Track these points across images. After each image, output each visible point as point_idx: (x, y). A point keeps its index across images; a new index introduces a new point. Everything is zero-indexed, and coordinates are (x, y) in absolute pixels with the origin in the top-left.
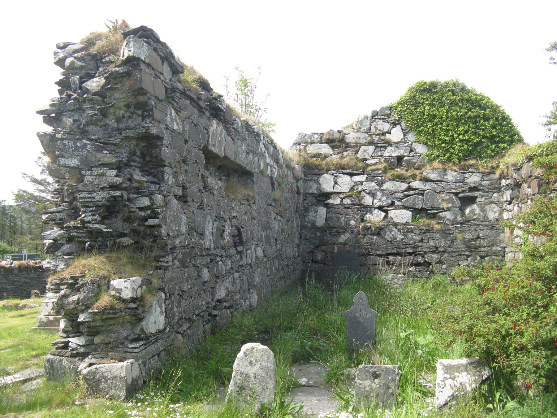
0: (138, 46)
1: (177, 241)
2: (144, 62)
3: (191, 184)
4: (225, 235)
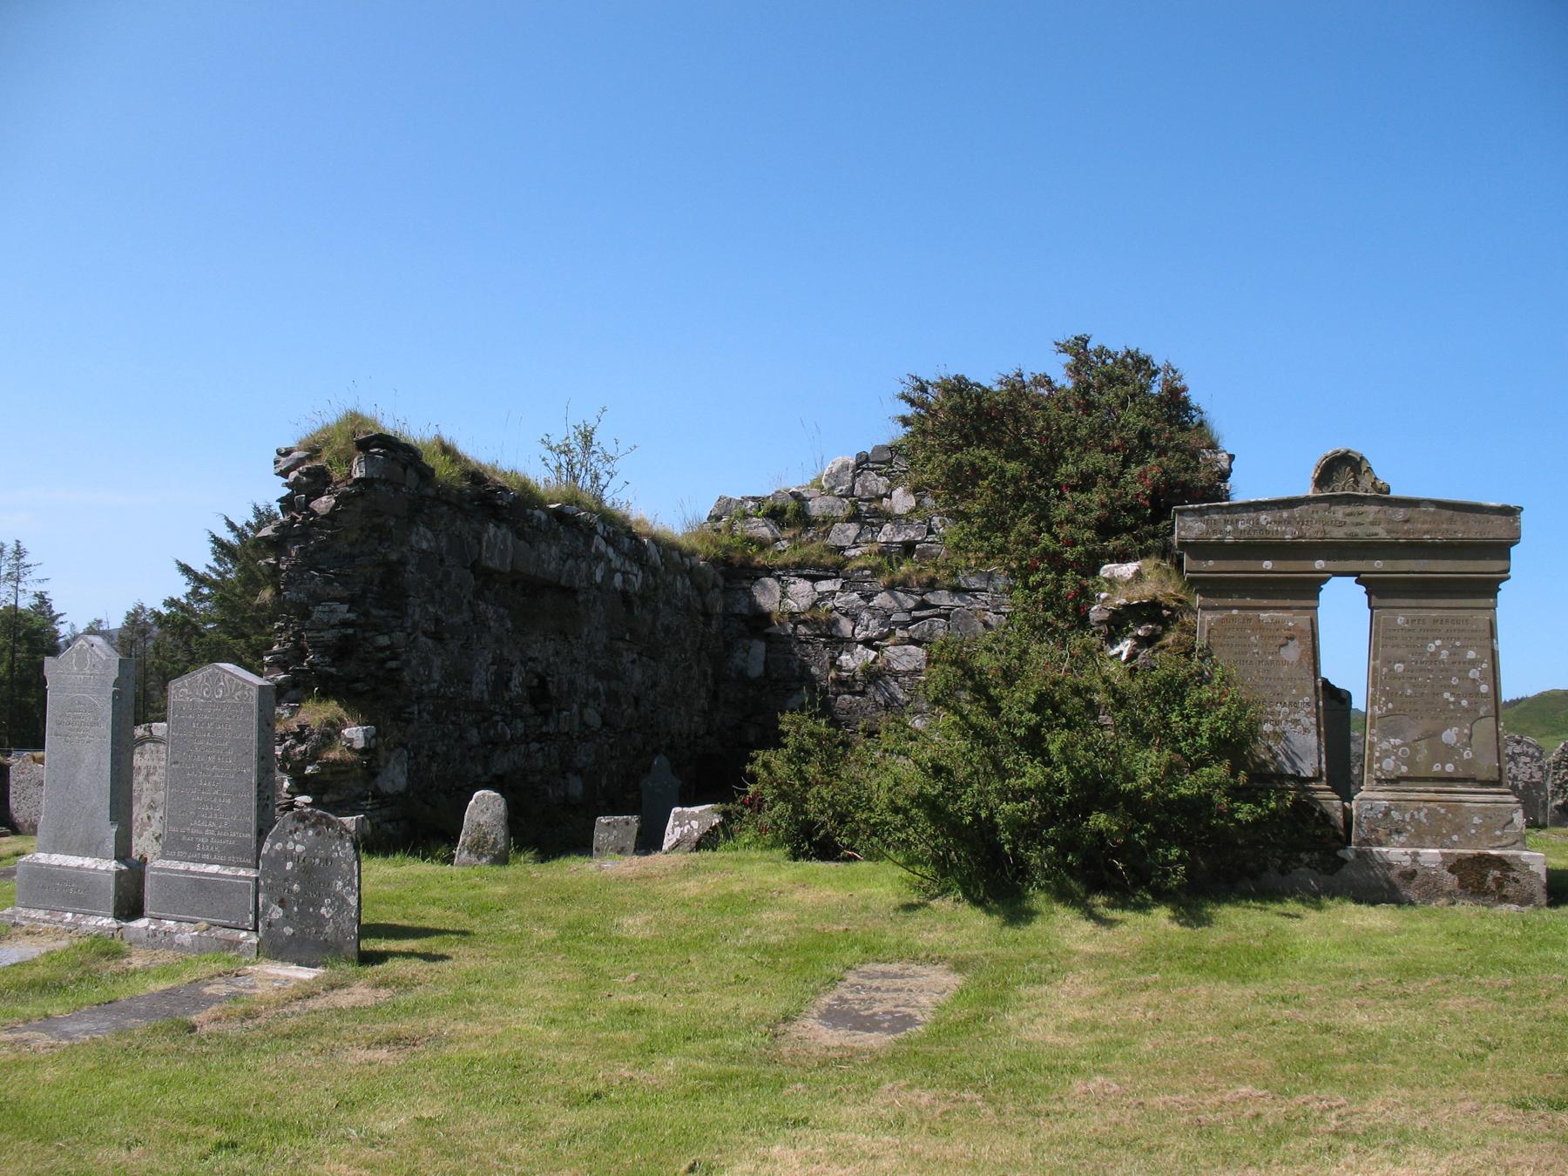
4: (512, 685)
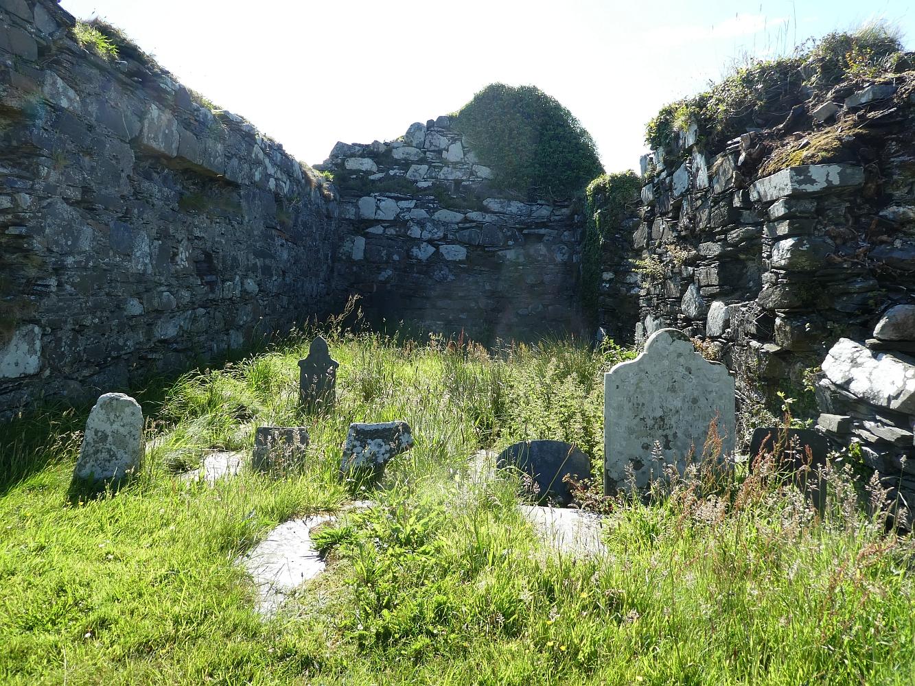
4: (177, 259)
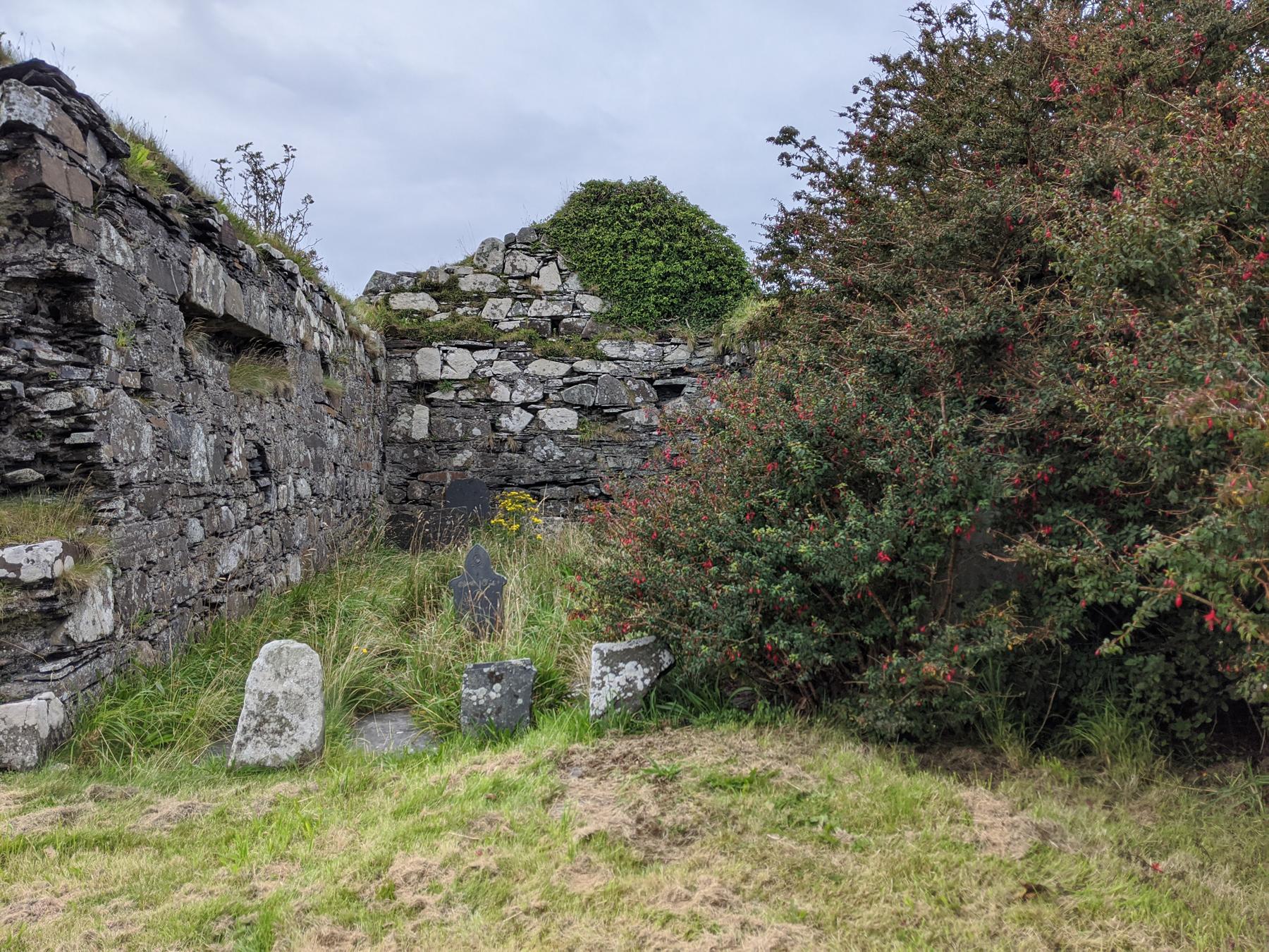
0: (28, 101)
1: (135, 472)
2: (44, 134)
3: (157, 368)
4: (232, 459)
